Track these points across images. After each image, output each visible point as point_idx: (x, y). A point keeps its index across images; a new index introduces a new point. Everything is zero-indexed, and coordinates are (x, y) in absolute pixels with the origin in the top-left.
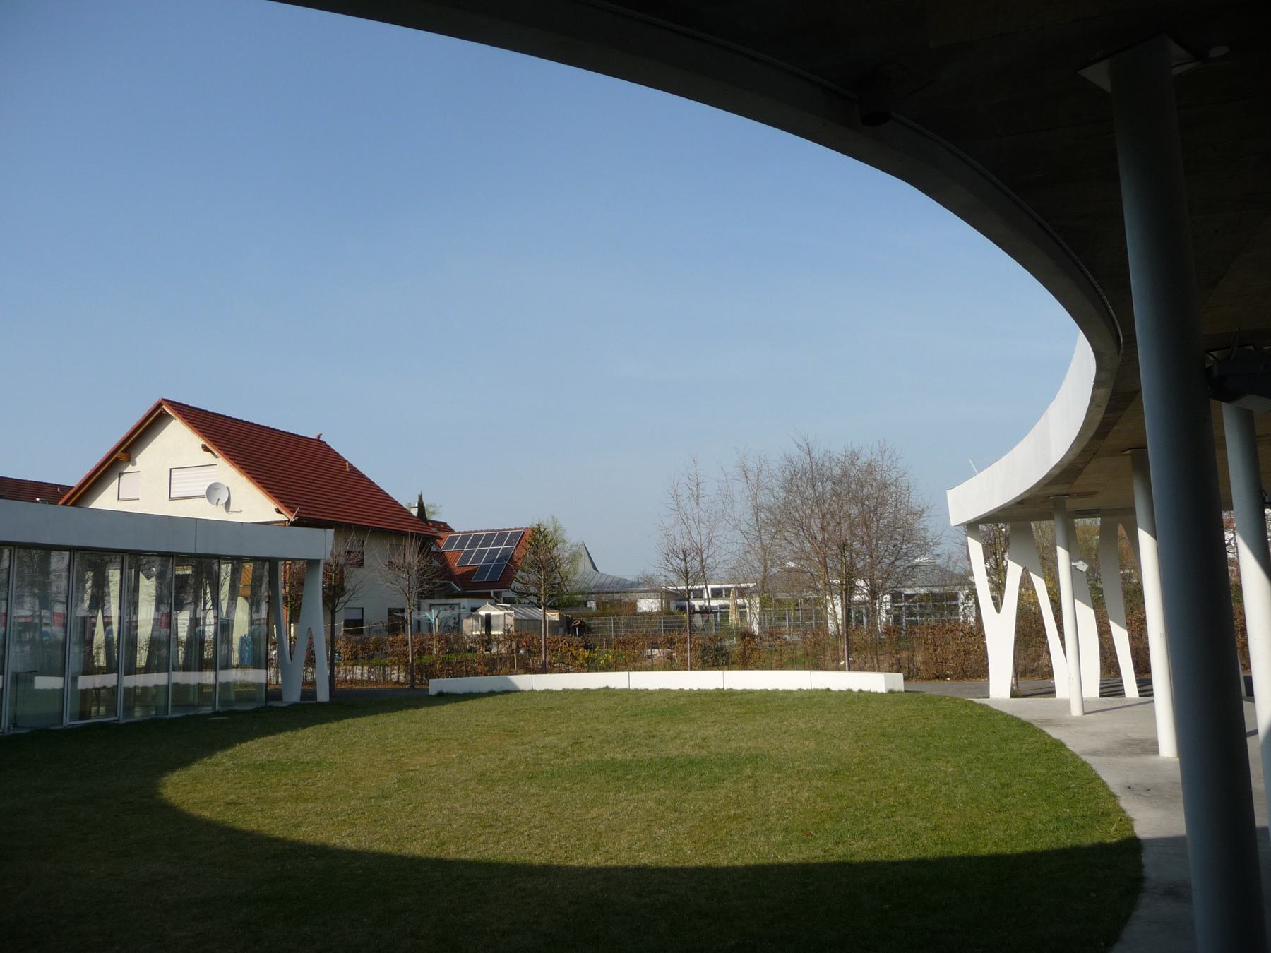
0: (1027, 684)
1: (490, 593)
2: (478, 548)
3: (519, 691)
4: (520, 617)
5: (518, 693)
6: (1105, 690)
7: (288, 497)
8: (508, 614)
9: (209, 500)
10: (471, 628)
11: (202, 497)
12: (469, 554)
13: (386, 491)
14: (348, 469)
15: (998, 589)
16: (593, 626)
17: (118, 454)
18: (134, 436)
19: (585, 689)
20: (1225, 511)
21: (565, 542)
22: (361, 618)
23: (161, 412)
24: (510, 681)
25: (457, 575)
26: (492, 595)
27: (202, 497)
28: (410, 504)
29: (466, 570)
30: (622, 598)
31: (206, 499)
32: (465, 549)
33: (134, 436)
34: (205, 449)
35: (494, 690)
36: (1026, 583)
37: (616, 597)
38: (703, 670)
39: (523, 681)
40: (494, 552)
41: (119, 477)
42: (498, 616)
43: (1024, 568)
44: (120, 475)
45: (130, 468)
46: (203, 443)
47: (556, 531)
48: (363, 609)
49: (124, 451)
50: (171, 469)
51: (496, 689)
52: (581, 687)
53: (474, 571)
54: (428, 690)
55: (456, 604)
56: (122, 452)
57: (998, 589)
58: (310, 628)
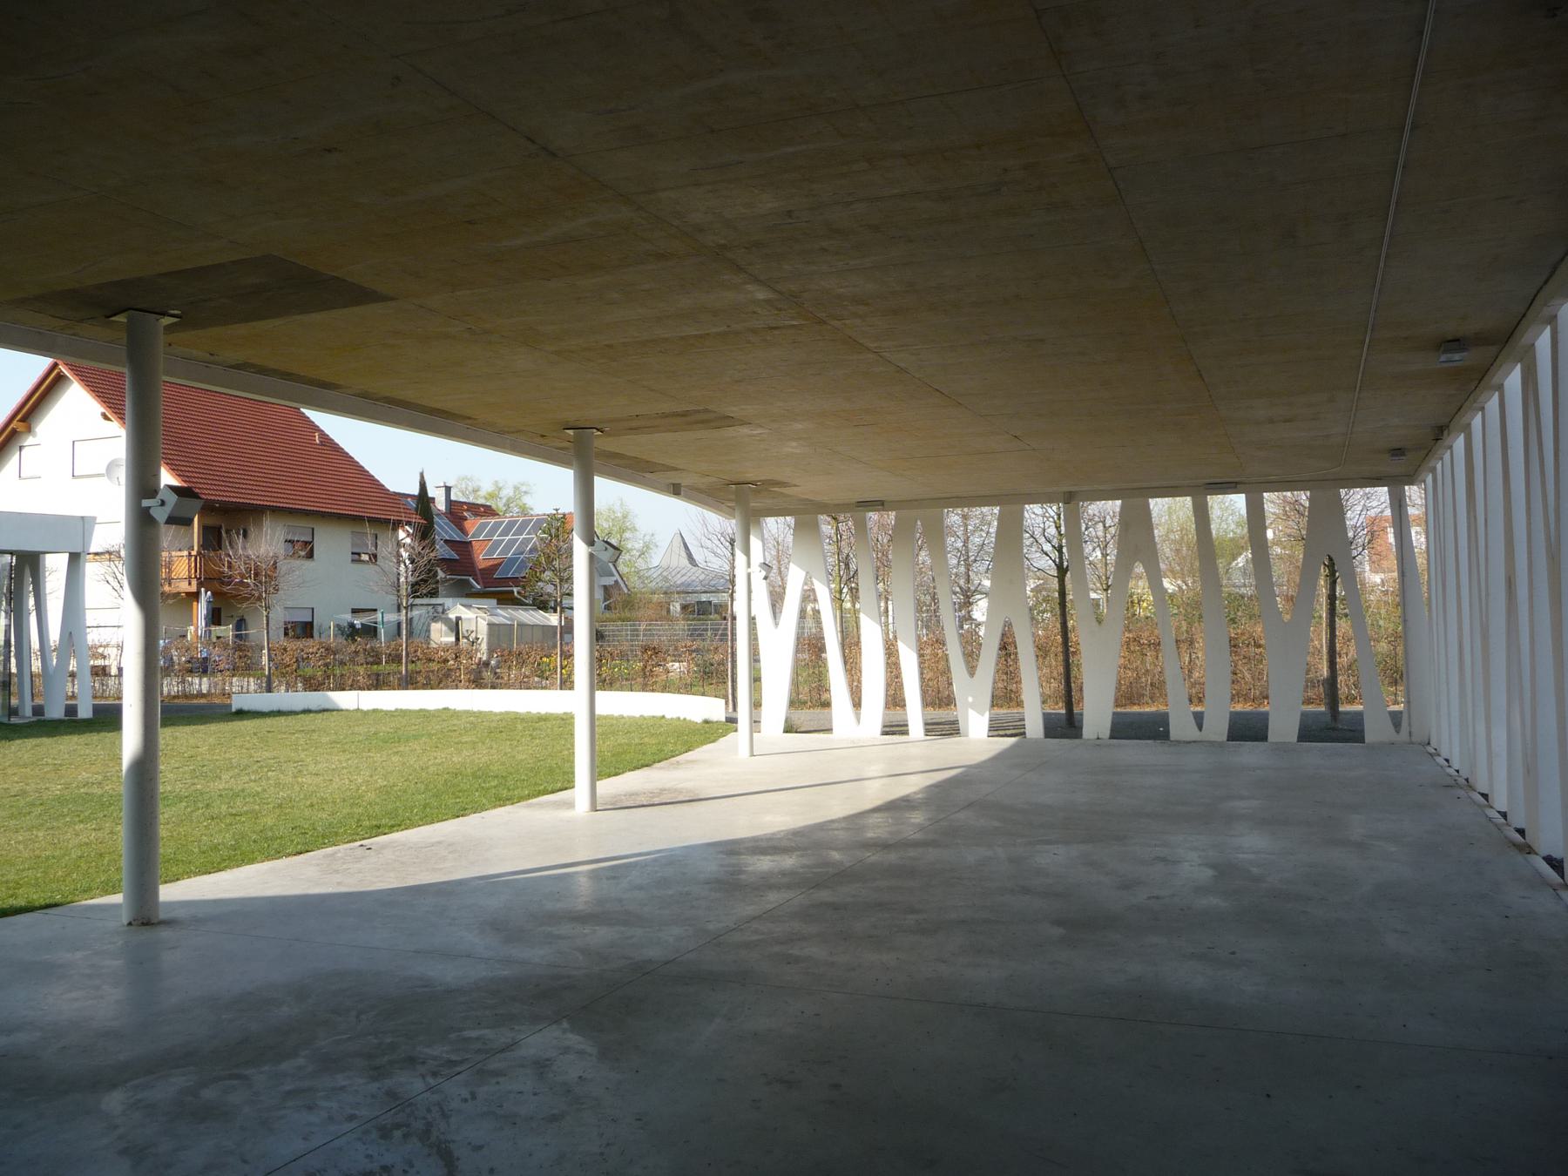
0: (804, 716)
1: (513, 592)
2: (509, 537)
3: (342, 710)
4: (496, 620)
5: (335, 713)
6: (888, 729)
7: (266, 471)
8: (480, 617)
9: (109, 478)
10: (440, 635)
11: (102, 475)
12: (498, 543)
13: (362, 463)
14: (318, 441)
15: (777, 599)
16: (607, 633)
17: (14, 424)
18: (31, 402)
19: (421, 710)
20: (1311, 499)
21: (634, 529)
22: (310, 620)
23: (58, 374)
24: (329, 699)
25: (480, 570)
26: (516, 593)
27: (102, 475)
28: (496, 482)
29: (491, 563)
30: (711, 599)
31: (106, 477)
32: (495, 538)
33: (31, 402)
34: (106, 417)
35: (281, 709)
36: (809, 596)
37: (704, 598)
38: (643, 690)
39: (346, 699)
40: (528, 540)
41: (20, 450)
42: (469, 619)
43: (807, 573)
44: (21, 448)
45: (30, 440)
46: (103, 410)
47: (625, 517)
48: (313, 609)
49: (23, 420)
50: (74, 442)
51: (284, 708)
52: (417, 708)
53: (500, 564)
54: (230, 705)
55: (440, 605)
56: (19, 421)
57: (777, 599)
58: (71, 633)
